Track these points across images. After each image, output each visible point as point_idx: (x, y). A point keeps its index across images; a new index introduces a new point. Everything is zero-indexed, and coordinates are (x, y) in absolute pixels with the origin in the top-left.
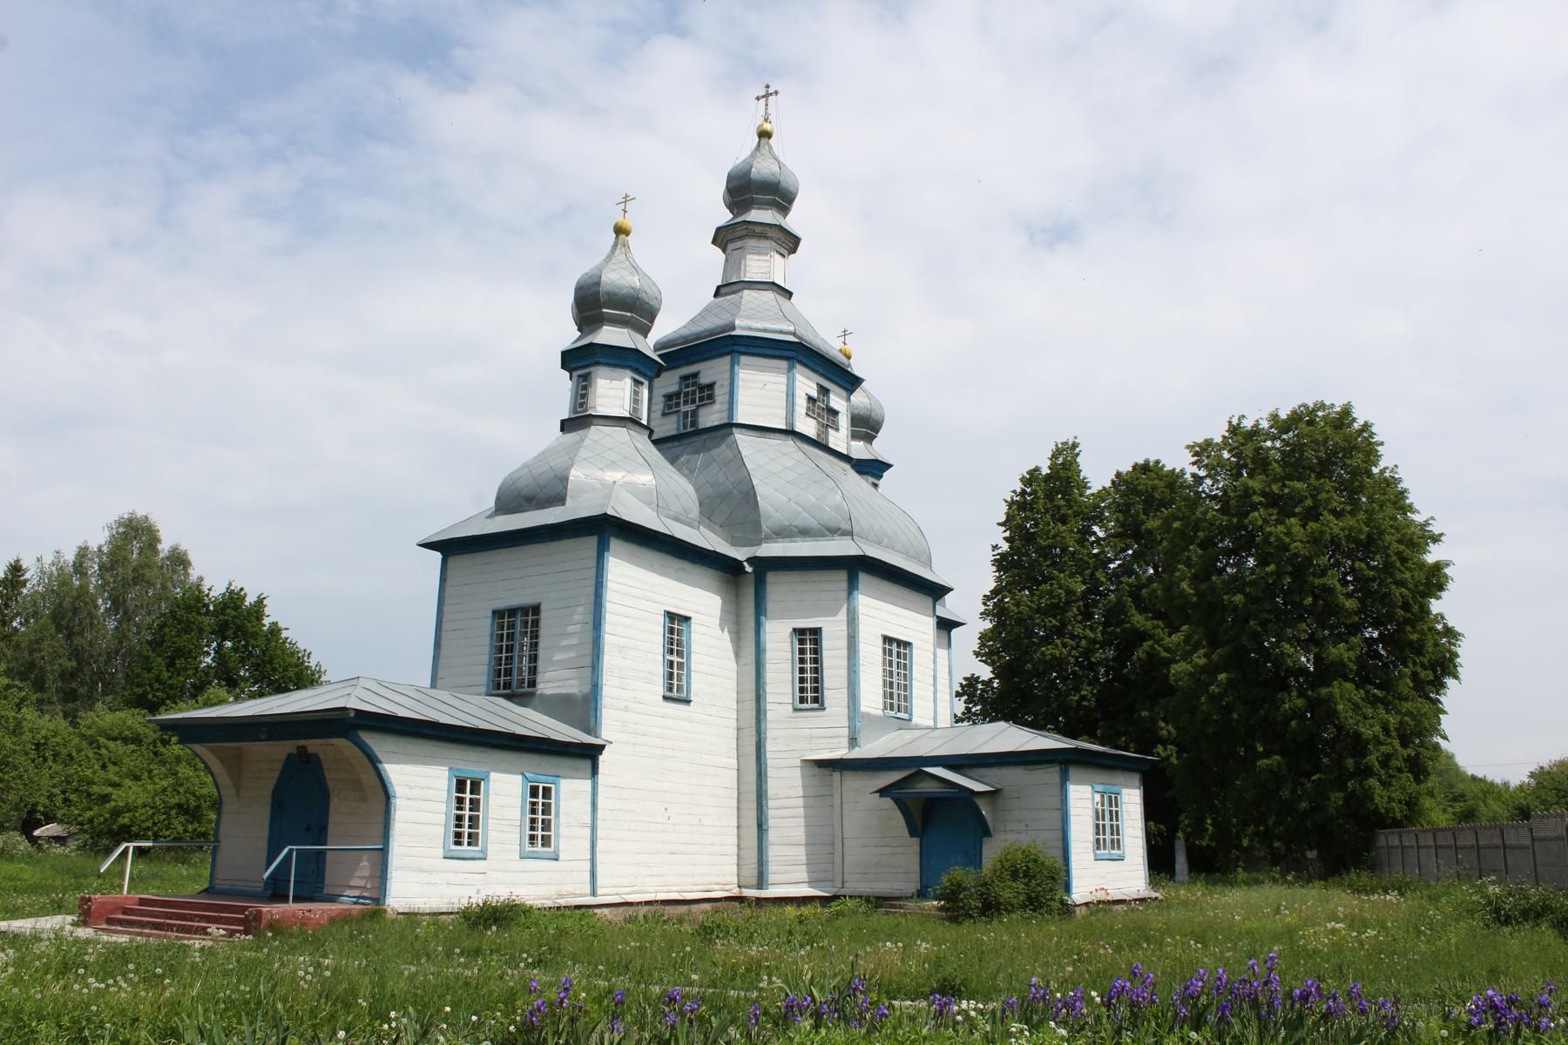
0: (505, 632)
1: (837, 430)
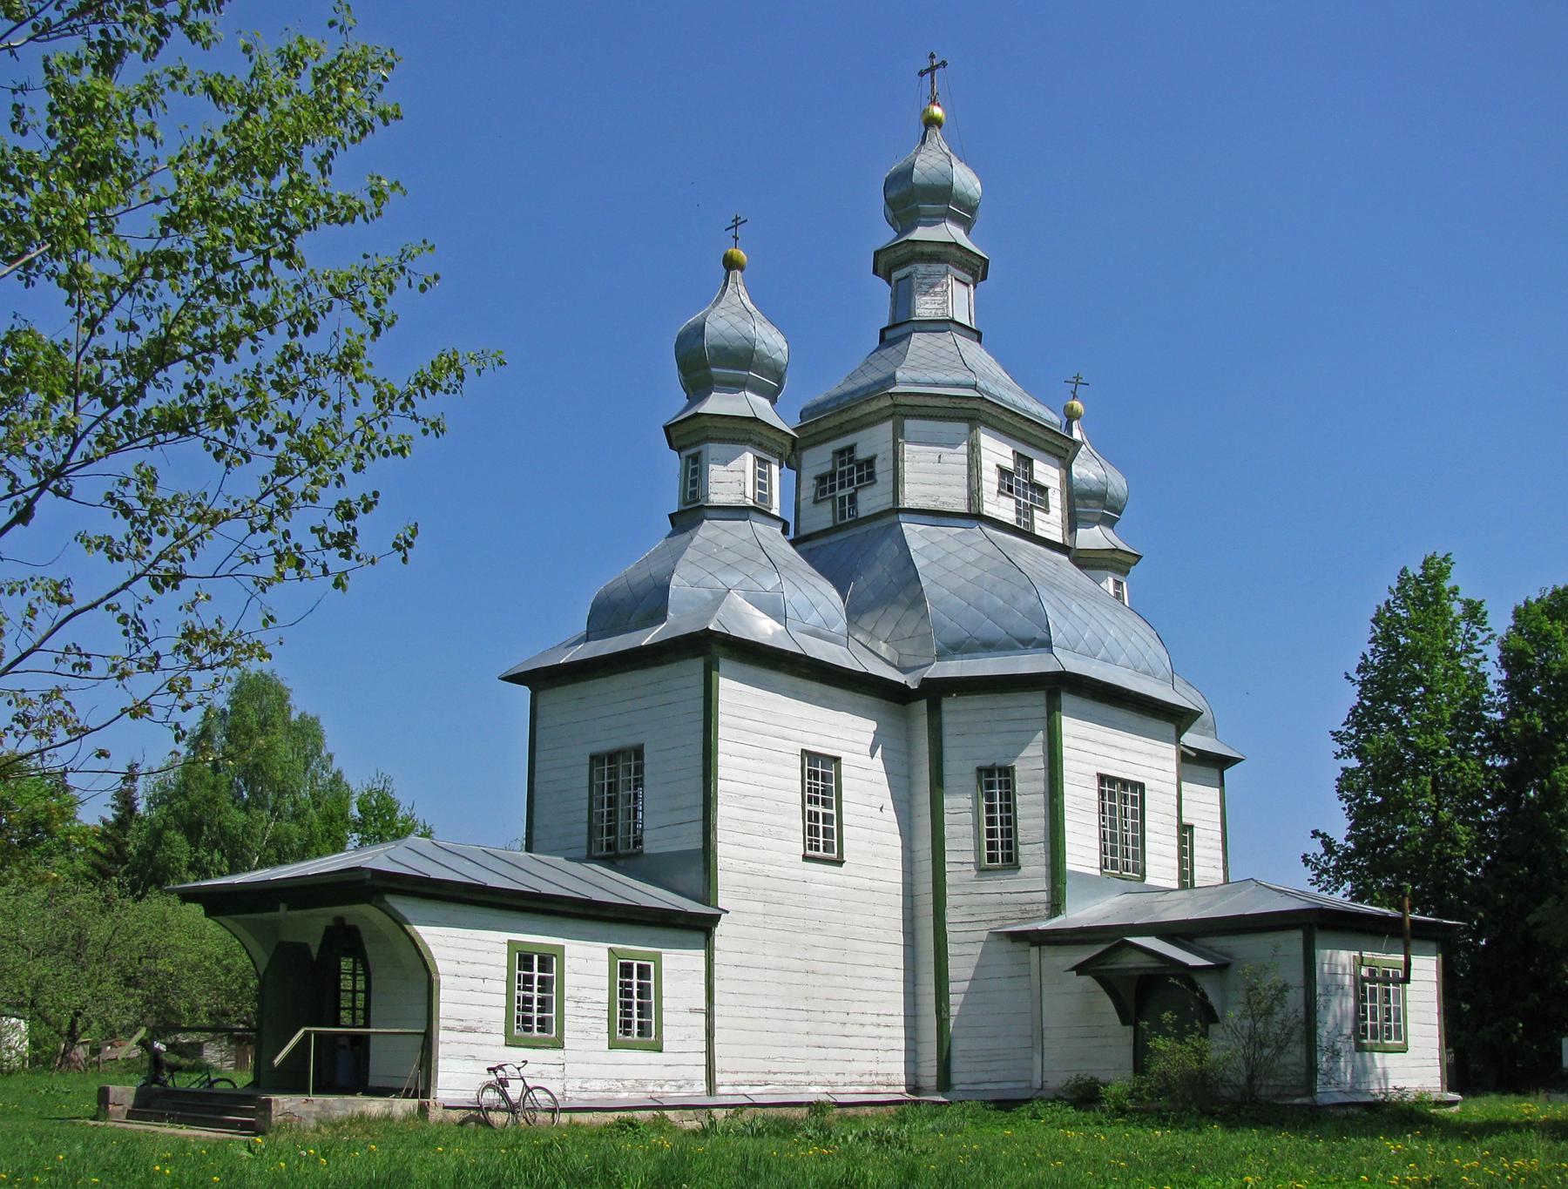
0: (606, 781)
1: (1047, 512)
